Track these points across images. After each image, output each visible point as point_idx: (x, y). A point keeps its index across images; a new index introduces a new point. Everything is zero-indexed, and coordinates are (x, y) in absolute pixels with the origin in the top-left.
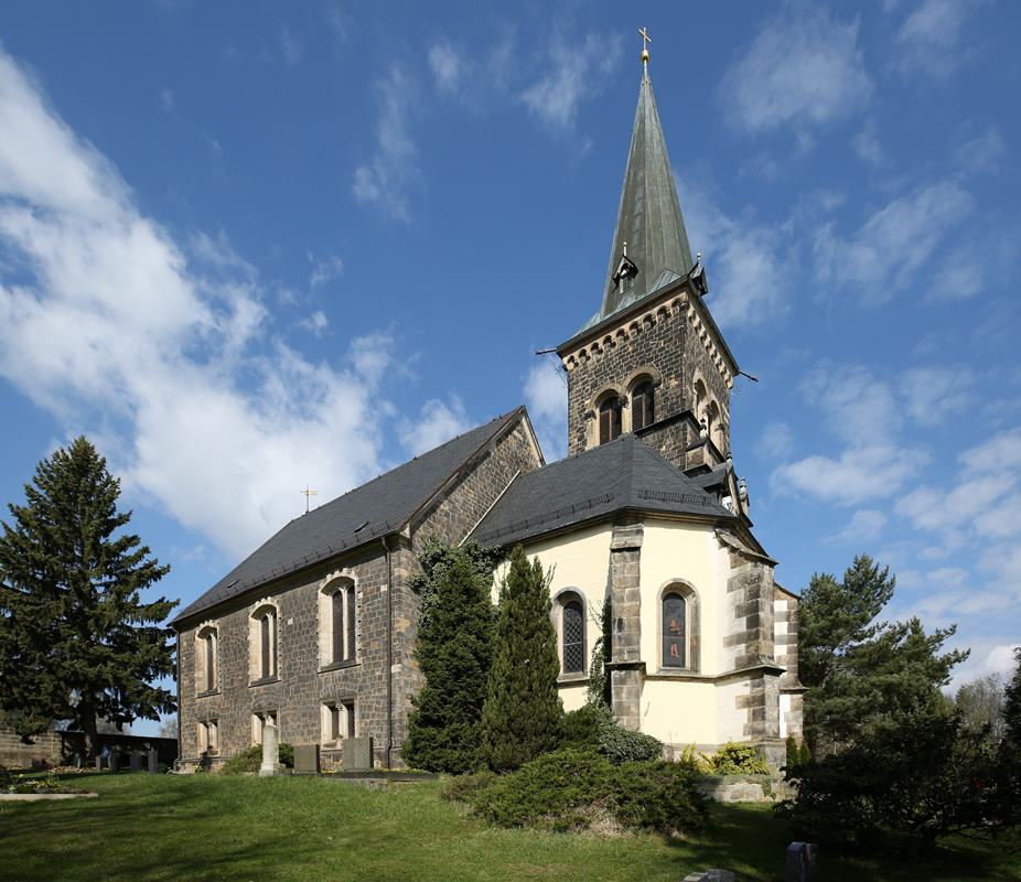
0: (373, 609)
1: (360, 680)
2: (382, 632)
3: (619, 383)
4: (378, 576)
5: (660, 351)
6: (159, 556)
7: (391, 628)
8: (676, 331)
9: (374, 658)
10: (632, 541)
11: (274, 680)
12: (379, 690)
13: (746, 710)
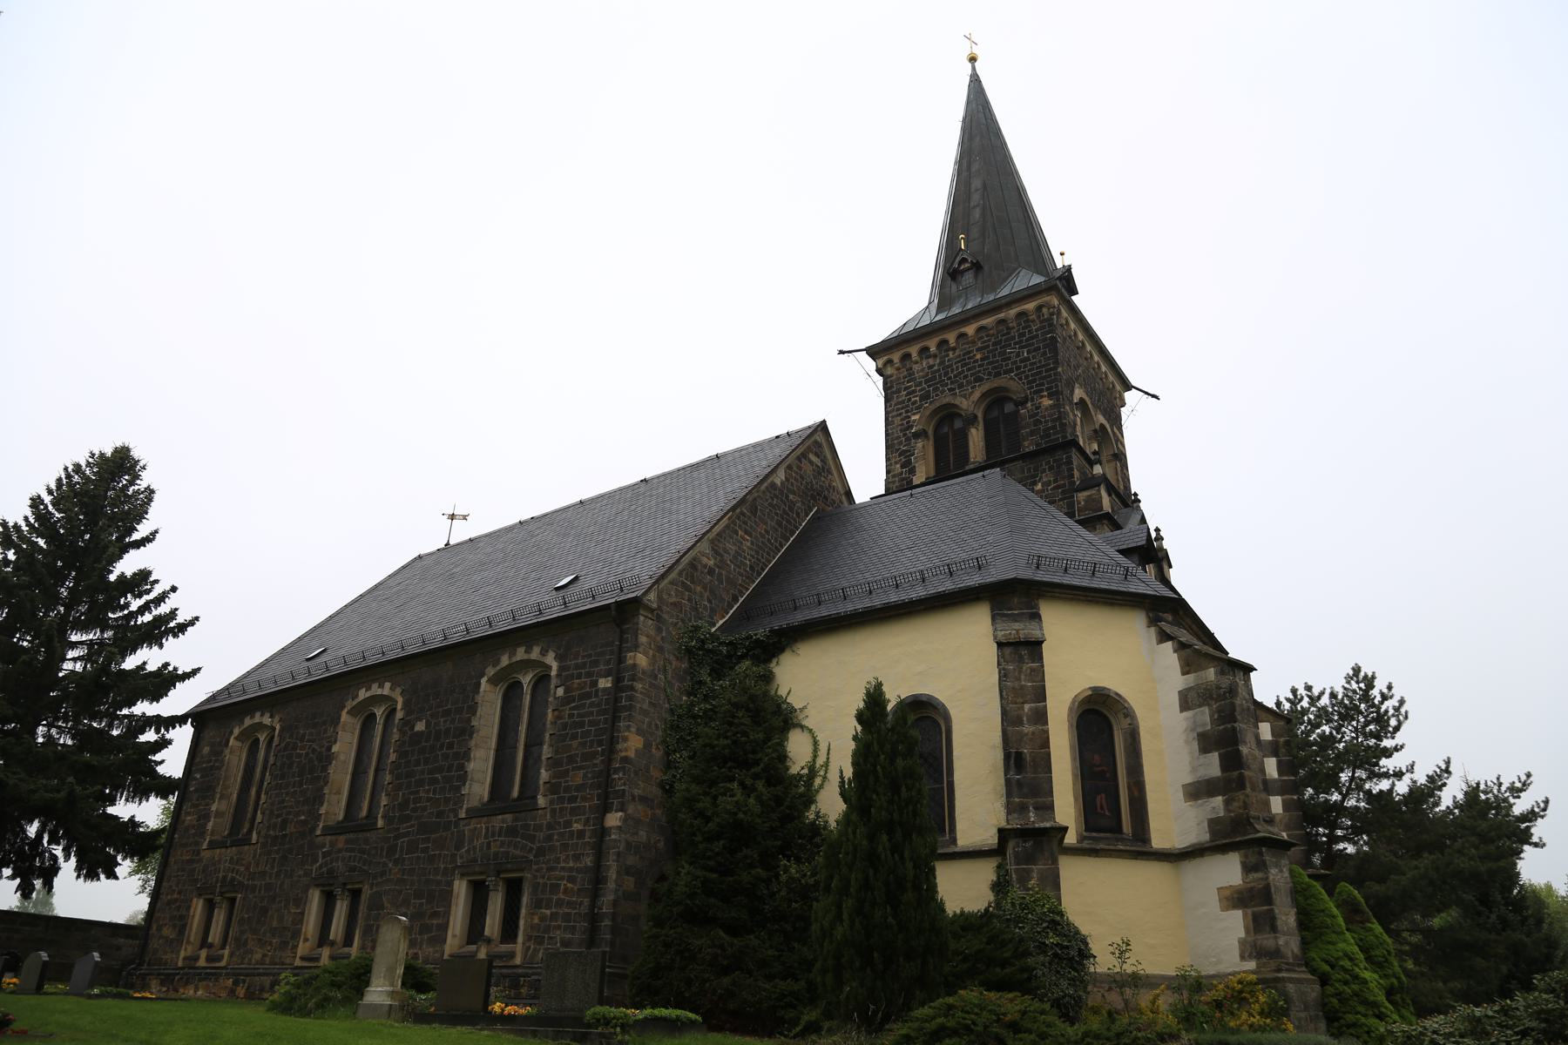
0: (580, 715)
1: (541, 835)
2: (594, 755)
4: (596, 663)
5: (1021, 361)
6: (183, 605)
7: (611, 750)
8: (1045, 340)
9: (573, 799)
10: (1024, 630)
11: (369, 825)
12: (577, 858)
13: (1238, 913)
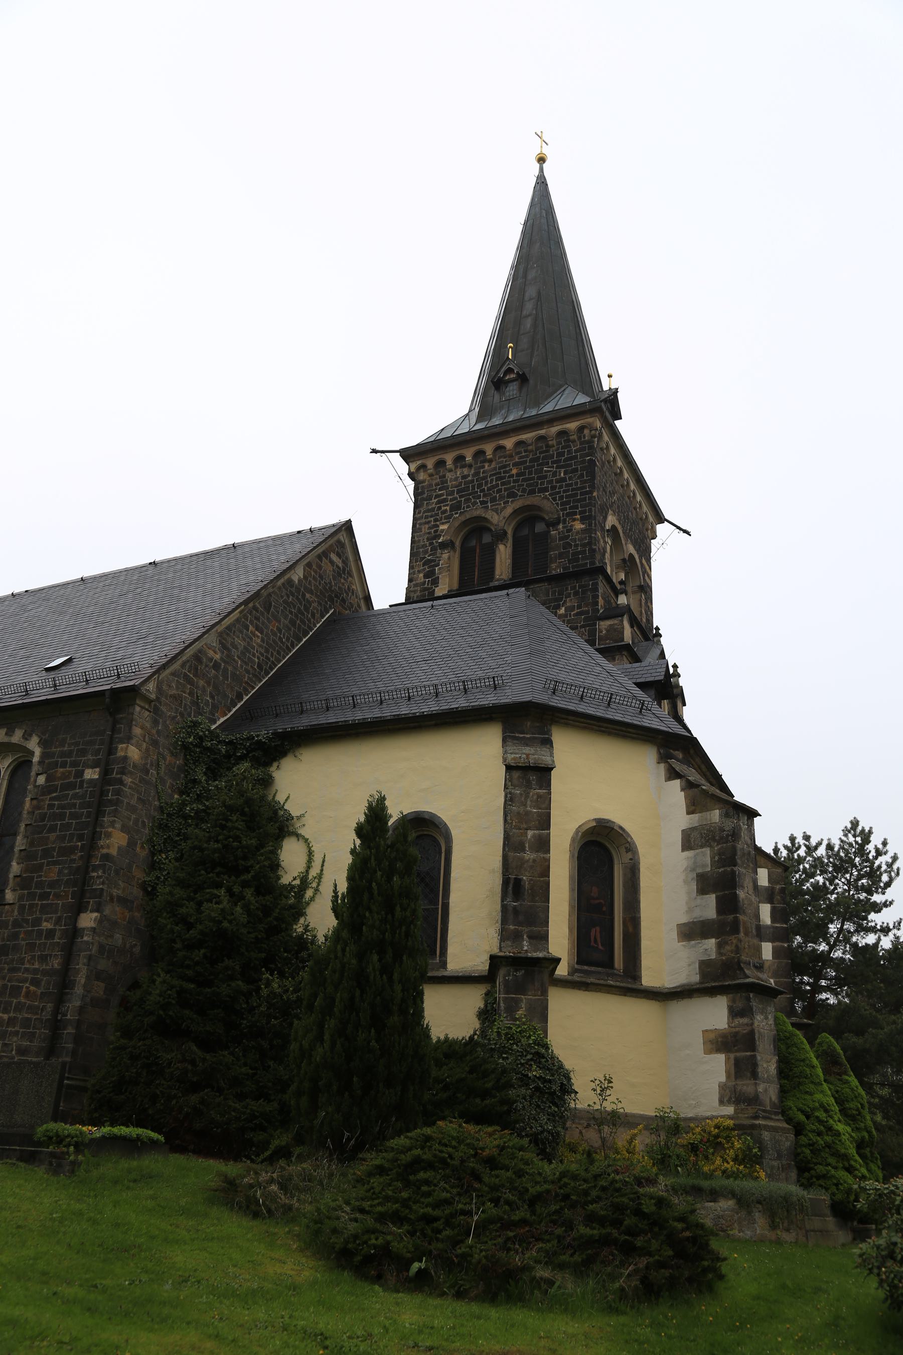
0: (62, 807)
2: (72, 850)
3: (496, 511)
4: (83, 752)
5: (557, 481)
8: (583, 462)
12: (43, 959)
13: (721, 1057)
